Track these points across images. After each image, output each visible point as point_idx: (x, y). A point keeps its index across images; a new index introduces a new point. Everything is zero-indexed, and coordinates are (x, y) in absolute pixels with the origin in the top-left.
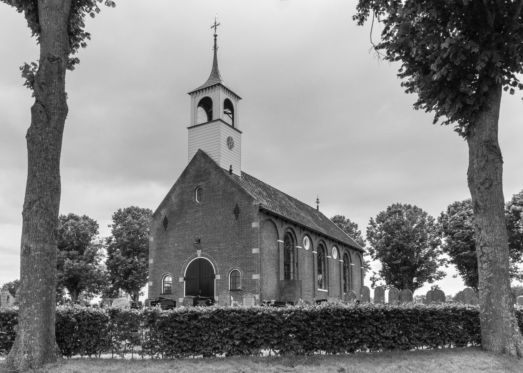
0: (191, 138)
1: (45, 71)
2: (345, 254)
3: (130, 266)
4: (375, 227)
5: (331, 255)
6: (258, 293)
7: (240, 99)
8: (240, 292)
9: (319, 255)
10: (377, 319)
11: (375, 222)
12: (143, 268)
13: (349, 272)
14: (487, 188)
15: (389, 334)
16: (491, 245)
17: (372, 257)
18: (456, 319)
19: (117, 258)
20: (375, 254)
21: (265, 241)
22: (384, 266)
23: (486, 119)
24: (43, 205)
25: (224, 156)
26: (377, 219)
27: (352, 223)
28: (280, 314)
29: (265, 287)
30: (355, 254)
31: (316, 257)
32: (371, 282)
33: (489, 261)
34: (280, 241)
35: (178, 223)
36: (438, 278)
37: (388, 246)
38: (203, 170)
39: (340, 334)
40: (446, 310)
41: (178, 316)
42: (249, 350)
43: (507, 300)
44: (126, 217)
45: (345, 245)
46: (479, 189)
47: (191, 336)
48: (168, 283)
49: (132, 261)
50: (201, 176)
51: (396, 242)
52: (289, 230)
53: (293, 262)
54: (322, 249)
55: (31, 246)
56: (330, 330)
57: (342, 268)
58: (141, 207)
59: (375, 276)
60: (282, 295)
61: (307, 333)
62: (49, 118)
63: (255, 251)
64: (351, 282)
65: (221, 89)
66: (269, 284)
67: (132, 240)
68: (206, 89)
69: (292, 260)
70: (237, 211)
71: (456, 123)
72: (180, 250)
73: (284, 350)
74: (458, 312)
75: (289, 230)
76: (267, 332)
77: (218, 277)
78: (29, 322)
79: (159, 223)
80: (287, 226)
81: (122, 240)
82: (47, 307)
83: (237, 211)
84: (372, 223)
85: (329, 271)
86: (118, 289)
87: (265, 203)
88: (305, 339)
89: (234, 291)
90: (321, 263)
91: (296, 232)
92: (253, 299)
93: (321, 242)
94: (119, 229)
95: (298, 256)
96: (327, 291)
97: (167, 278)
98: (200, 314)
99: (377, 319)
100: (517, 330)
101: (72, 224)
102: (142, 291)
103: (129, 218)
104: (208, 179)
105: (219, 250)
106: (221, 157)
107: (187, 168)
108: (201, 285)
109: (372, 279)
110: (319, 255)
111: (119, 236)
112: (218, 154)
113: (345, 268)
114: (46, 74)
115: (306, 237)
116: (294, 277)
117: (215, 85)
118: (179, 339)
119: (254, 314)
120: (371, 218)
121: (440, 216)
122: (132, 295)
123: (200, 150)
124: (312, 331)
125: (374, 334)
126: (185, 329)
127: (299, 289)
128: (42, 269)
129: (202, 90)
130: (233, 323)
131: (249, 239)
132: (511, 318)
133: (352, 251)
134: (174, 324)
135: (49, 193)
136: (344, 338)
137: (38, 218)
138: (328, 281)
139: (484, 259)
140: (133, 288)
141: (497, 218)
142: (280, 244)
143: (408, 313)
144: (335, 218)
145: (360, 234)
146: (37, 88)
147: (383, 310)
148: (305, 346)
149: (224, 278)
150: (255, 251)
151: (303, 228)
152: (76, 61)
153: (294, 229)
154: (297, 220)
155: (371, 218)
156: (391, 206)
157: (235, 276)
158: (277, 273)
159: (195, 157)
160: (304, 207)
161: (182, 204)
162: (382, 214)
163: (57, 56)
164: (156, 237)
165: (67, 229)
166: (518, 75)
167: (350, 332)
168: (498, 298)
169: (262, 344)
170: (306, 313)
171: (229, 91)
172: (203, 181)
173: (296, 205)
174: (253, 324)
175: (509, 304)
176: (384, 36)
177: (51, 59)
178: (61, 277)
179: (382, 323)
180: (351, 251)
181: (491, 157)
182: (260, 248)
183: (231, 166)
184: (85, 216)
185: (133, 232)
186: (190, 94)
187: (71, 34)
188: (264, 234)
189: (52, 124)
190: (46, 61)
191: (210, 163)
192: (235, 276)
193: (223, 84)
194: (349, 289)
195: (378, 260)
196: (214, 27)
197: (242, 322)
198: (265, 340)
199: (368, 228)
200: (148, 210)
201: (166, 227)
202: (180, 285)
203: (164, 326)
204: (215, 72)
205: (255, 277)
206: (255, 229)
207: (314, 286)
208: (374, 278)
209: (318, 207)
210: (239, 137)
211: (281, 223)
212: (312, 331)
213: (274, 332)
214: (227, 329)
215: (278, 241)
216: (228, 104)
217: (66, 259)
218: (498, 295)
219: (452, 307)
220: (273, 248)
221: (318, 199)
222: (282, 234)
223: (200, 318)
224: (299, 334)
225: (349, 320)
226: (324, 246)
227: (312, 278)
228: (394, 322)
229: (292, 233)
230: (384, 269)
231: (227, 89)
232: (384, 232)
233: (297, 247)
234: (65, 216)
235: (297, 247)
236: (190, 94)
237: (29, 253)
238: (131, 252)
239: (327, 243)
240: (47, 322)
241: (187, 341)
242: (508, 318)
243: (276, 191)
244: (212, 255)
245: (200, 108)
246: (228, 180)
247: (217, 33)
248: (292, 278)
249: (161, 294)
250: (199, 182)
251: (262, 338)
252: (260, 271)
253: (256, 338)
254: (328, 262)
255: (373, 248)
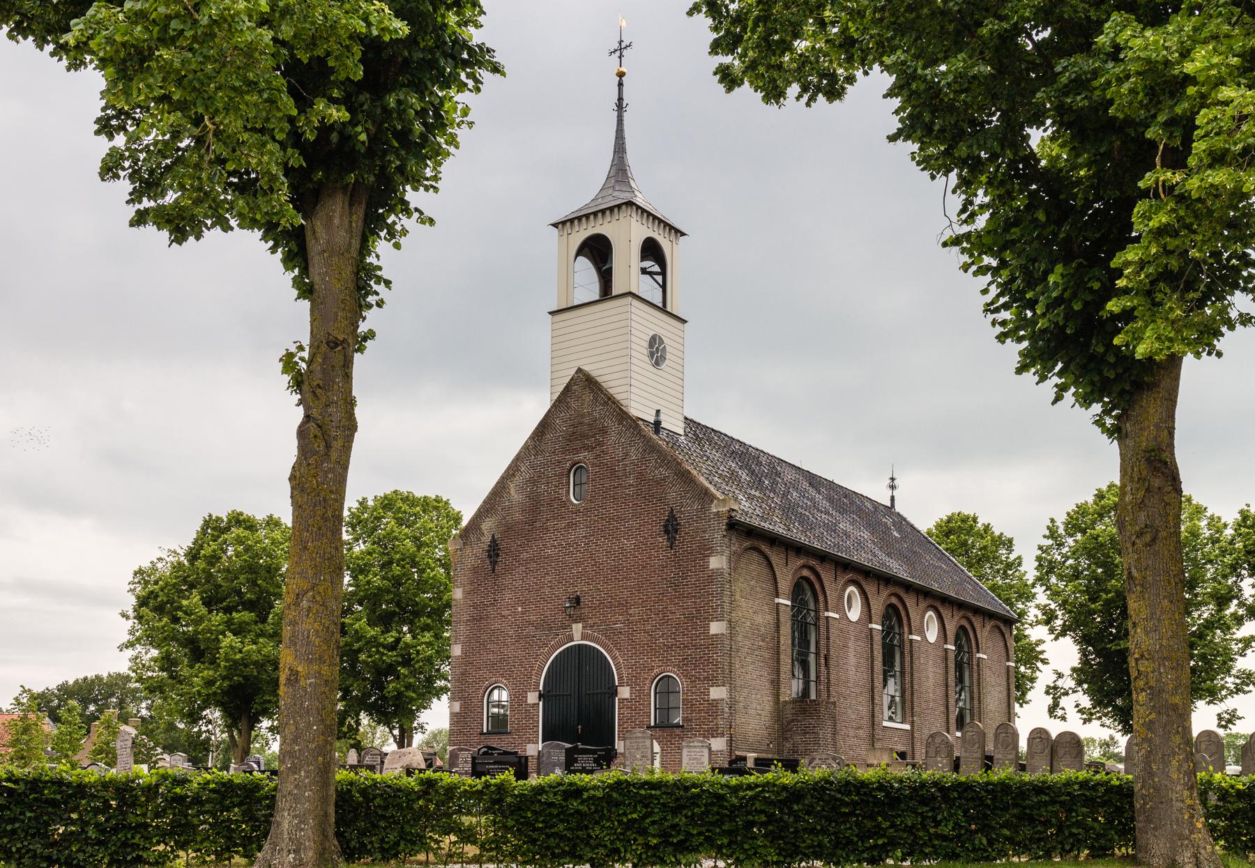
0: (560, 339)
1: (322, 365)
2: (962, 628)
3: (391, 657)
4: (1061, 545)
5: (921, 632)
6: (722, 735)
7: (683, 234)
8: (678, 731)
9: (888, 633)
10: (924, 801)
11: (1061, 531)
12: (429, 660)
13: (971, 677)
14: (1147, 545)
15: (946, 829)
16: (1153, 658)
17: (1052, 631)
18: (1090, 802)
19: (356, 631)
20: (1059, 622)
21: (743, 602)
22: (1084, 653)
23: (1151, 406)
24: (318, 599)
25: (639, 378)
26: (1066, 524)
27: (997, 533)
28: (735, 789)
29: (740, 719)
30: (988, 627)
31: (878, 639)
32: (1049, 700)
33: (1150, 688)
34: (781, 601)
35: (525, 555)
36: (1238, 690)
37: (1093, 600)
38: (586, 420)
39: (850, 828)
40: (1068, 783)
41: (547, 792)
42: (675, 856)
43: (1180, 765)
44: (378, 519)
45: (960, 605)
46: (1134, 544)
47: (568, 829)
48: (498, 706)
49: (398, 640)
50: (584, 421)
51: (1117, 592)
52: (806, 573)
53: (817, 654)
54: (895, 618)
55: (300, 669)
56: (831, 822)
57: (952, 665)
58: (419, 494)
59: (1060, 683)
60: (786, 739)
61: (787, 826)
62: (328, 447)
63: (716, 628)
64: (976, 702)
65: (634, 215)
66: (752, 712)
67: (397, 582)
68: (595, 214)
69: (813, 649)
70: (671, 528)
71: (1097, 408)
72: (530, 623)
73: (742, 857)
74: (1094, 788)
75: (806, 573)
76: (711, 824)
77: (624, 692)
78: (297, 799)
79: (475, 553)
80: (800, 562)
81: (369, 582)
82: (325, 771)
83: (671, 528)
84: (1053, 534)
85: (916, 675)
86: (358, 715)
87: (745, 505)
88: (782, 838)
89: (664, 727)
90: (893, 651)
91: (823, 575)
92: (706, 751)
93: (894, 600)
94: (362, 553)
95: (828, 638)
96: (907, 727)
97: (496, 692)
98: (586, 789)
99: (924, 801)
100: (1199, 826)
101: (239, 541)
102: (421, 720)
103: (389, 522)
104: (600, 444)
105: (628, 622)
106: (633, 389)
107: (547, 415)
108: (581, 714)
109: (1052, 690)
110: (888, 633)
111: (362, 571)
112: (626, 381)
113: (959, 667)
114: (323, 371)
115: (852, 589)
116: (818, 692)
117: (619, 206)
118: (546, 834)
119: (687, 789)
120: (1052, 521)
121: (1239, 517)
122: (396, 732)
123: (579, 370)
124: (796, 822)
125: (918, 830)
126: (558, 815)
127: (829, 723)
128: (317, 709)
129: (587, 216)
130: (646, 806)
131: (703, 597)
132: (1189, 802)
133: (985, 622)
134: (537, 808)
135: (328, 577)
136: (857, 835)
137: (311, 621)
138: (912, 702)
139: (1141, 683)
140: (399, 713)
141: (1166, 603)
142: (782, 608)
143: (987, 791)
144: (950, 520)
145: (1020, 564)
146: (309, 396)
147: (935, 784)
148: (782, 849)
149: (640, 696)
150: (716, 628)
151: (844, 566)
152: (371, 335)
153: (819, 569)
154: (824, 543)
155: (1052, 521)
156: (1105, 488)
157: (666, 688)
158: (772, 682)
159: (568, 388)
160: (852, 503)
161: (534, 506)
162: (1082, 510)
163: (341, 337)
164: (468, 588)
165: (225, 552)
166: (1240, 302)
167: (869, 824)
168: (1164, 762)
169: (701, 844)
170: (784, 788)
171: (655, 218)
172: (590, 448)
173: (830, 500)
174: (684, 807)
175: (1186, 773)
176: (964, 216)
177: (333, 344)
178: (209, 683)
179: (933, 809)
180: (977, 622)
181: (1156, 483)
182: (730, 621)
183: (658, 411)
184: (271, 517)
185: (399, 561)
186: (555, 225)
187: (359, 289)
188: (740, 586)
189: (334, 455)
190: (324, 348)
191: (606, 403)
192: (666, 688)
193: (639, 201)
194: (972, 719)
195: (1068, 638)
196: (618, 53)
197: (664, 805)
198: (707, 838)
199: (1040, 548)
200: (438, 500)
201: (494, 563)
202: (530, 711)
203: (520, 809)
204: (620, 171)
205: (717, 693)
206: (718, 572)
207: (873, 716)
208: (1055, 688)
209: (893, 499)
210: (681, 334)
211: (783, 556)
212: (796, 822)
213: (723, 823)
214: (635, 816)
215: (777, 600)
216: (651, 250)
217: (223, 633)
218: (1164, 755)
219: (1081, 778)
220: (764, 619)
221: (893, 479)
222: (785, 584)
223: (585, 795)
224: (770, 828)
225: (868, 802)
226: (901, 609)
227: (867, 695)
228: (959, 807)
229: (812, 577)
230: (1085, 661)
231: (649, 214)
232: (1084, 563)
233: (826, 614)
234: (218, 519)
235: (826, 614)
236: (555, 225)
237: (297, 681)
238: (394, 614)
239: (910, 601)
240: (324, 800)
241: (562, 838)
242: (1182, 801)
243: (776, 464)
244: (611, 636)
245: (580, 258)
246: (651, 448)
247: (623, 69)
248: (813, 697)
249: (482, 734)
250: (577, 451)
251: (700, 834)
252: (728, 679)
253: (689, 834)
254: (911, 651)
255: (1053, 606)
